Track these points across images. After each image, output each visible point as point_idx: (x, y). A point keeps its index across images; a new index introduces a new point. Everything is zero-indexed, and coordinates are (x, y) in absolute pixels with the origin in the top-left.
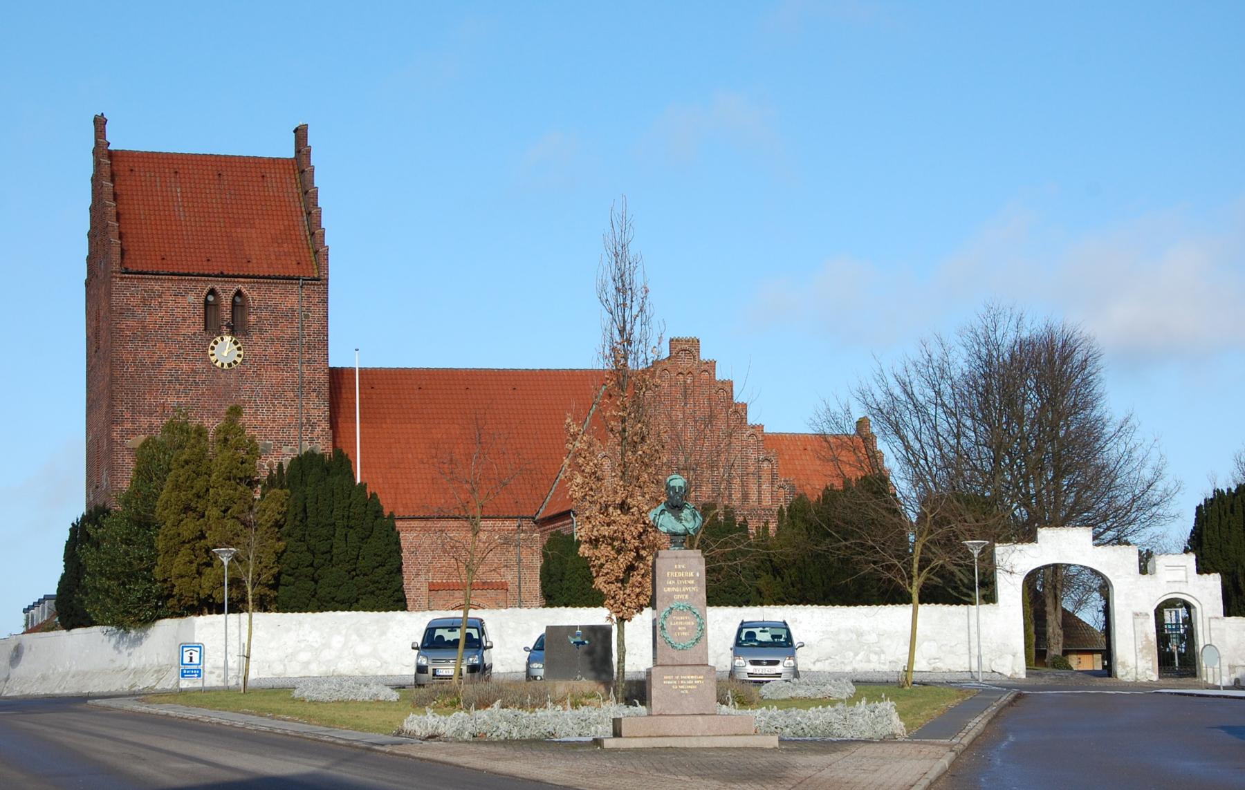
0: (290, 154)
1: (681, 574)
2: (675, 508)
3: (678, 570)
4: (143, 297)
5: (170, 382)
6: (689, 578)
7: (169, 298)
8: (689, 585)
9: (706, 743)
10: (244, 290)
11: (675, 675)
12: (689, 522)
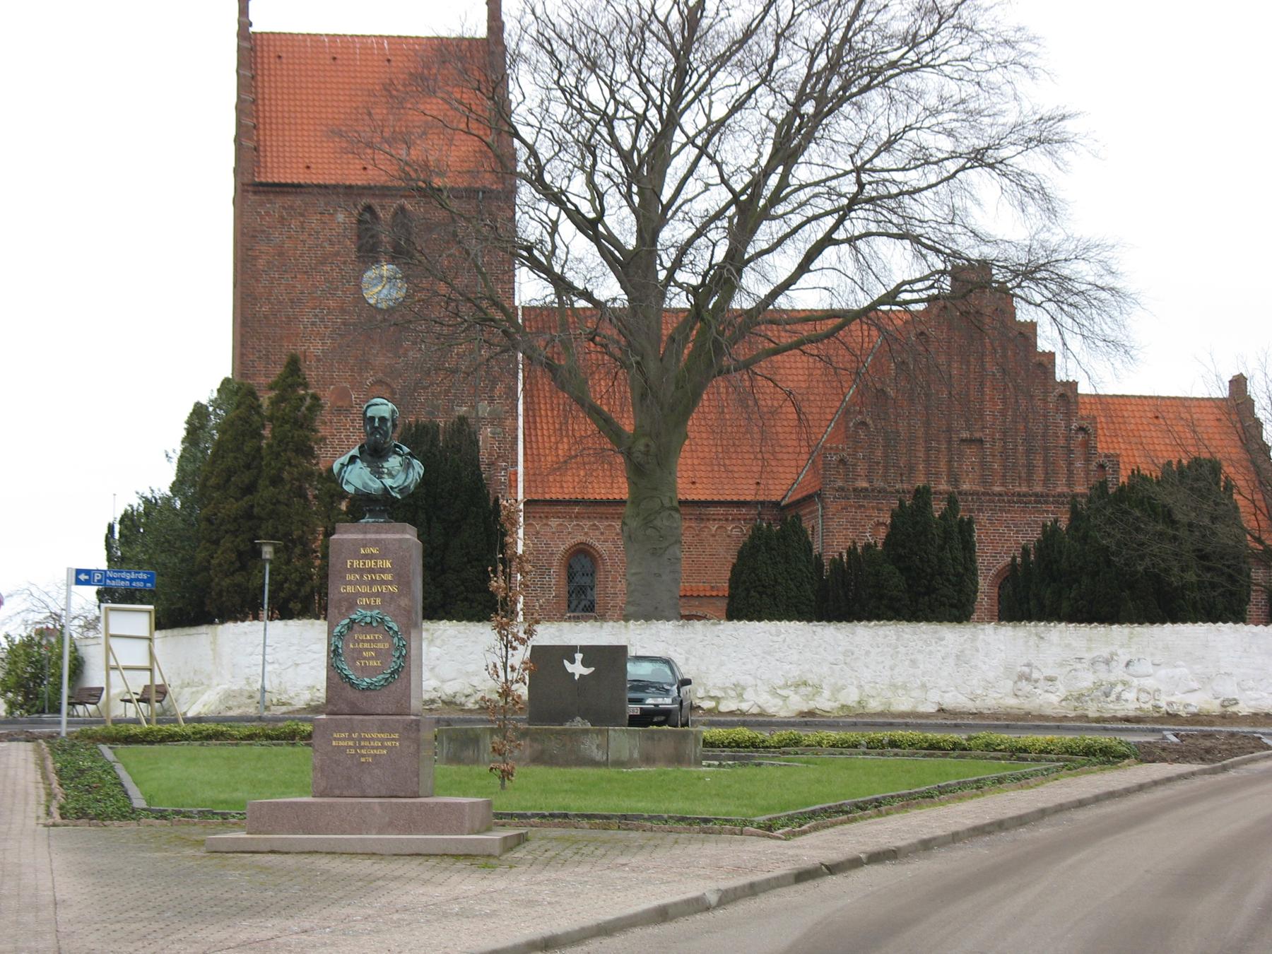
0: (482, 32)
1: (370, 564)
2: (374, 453)
3: (366, 556)
4: (282, 217)
5: (313, 324)
6: (383, 571)
7: (314, 221)
8: (383, 582)
9: (1082, 855)
10: (409, 207)
11: (351, 731)
12: (401, 473)
